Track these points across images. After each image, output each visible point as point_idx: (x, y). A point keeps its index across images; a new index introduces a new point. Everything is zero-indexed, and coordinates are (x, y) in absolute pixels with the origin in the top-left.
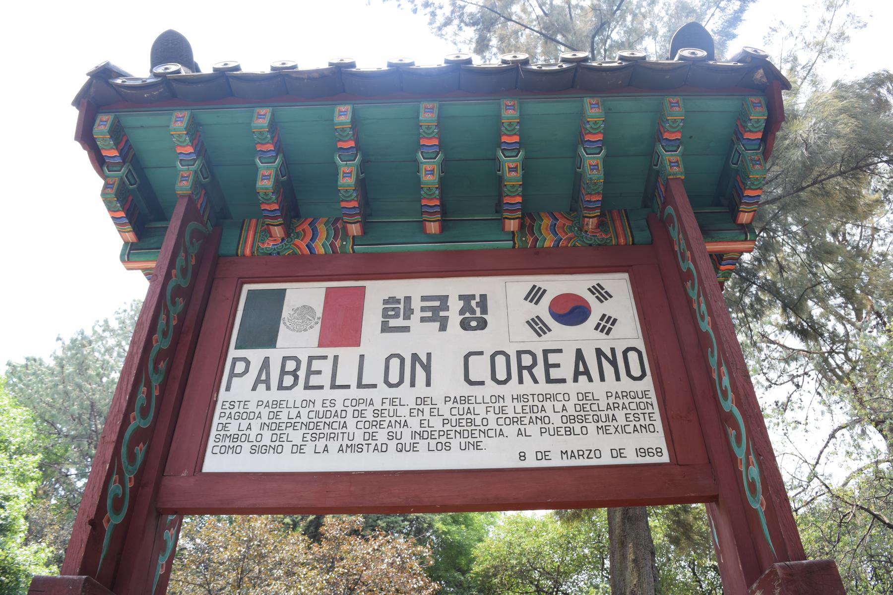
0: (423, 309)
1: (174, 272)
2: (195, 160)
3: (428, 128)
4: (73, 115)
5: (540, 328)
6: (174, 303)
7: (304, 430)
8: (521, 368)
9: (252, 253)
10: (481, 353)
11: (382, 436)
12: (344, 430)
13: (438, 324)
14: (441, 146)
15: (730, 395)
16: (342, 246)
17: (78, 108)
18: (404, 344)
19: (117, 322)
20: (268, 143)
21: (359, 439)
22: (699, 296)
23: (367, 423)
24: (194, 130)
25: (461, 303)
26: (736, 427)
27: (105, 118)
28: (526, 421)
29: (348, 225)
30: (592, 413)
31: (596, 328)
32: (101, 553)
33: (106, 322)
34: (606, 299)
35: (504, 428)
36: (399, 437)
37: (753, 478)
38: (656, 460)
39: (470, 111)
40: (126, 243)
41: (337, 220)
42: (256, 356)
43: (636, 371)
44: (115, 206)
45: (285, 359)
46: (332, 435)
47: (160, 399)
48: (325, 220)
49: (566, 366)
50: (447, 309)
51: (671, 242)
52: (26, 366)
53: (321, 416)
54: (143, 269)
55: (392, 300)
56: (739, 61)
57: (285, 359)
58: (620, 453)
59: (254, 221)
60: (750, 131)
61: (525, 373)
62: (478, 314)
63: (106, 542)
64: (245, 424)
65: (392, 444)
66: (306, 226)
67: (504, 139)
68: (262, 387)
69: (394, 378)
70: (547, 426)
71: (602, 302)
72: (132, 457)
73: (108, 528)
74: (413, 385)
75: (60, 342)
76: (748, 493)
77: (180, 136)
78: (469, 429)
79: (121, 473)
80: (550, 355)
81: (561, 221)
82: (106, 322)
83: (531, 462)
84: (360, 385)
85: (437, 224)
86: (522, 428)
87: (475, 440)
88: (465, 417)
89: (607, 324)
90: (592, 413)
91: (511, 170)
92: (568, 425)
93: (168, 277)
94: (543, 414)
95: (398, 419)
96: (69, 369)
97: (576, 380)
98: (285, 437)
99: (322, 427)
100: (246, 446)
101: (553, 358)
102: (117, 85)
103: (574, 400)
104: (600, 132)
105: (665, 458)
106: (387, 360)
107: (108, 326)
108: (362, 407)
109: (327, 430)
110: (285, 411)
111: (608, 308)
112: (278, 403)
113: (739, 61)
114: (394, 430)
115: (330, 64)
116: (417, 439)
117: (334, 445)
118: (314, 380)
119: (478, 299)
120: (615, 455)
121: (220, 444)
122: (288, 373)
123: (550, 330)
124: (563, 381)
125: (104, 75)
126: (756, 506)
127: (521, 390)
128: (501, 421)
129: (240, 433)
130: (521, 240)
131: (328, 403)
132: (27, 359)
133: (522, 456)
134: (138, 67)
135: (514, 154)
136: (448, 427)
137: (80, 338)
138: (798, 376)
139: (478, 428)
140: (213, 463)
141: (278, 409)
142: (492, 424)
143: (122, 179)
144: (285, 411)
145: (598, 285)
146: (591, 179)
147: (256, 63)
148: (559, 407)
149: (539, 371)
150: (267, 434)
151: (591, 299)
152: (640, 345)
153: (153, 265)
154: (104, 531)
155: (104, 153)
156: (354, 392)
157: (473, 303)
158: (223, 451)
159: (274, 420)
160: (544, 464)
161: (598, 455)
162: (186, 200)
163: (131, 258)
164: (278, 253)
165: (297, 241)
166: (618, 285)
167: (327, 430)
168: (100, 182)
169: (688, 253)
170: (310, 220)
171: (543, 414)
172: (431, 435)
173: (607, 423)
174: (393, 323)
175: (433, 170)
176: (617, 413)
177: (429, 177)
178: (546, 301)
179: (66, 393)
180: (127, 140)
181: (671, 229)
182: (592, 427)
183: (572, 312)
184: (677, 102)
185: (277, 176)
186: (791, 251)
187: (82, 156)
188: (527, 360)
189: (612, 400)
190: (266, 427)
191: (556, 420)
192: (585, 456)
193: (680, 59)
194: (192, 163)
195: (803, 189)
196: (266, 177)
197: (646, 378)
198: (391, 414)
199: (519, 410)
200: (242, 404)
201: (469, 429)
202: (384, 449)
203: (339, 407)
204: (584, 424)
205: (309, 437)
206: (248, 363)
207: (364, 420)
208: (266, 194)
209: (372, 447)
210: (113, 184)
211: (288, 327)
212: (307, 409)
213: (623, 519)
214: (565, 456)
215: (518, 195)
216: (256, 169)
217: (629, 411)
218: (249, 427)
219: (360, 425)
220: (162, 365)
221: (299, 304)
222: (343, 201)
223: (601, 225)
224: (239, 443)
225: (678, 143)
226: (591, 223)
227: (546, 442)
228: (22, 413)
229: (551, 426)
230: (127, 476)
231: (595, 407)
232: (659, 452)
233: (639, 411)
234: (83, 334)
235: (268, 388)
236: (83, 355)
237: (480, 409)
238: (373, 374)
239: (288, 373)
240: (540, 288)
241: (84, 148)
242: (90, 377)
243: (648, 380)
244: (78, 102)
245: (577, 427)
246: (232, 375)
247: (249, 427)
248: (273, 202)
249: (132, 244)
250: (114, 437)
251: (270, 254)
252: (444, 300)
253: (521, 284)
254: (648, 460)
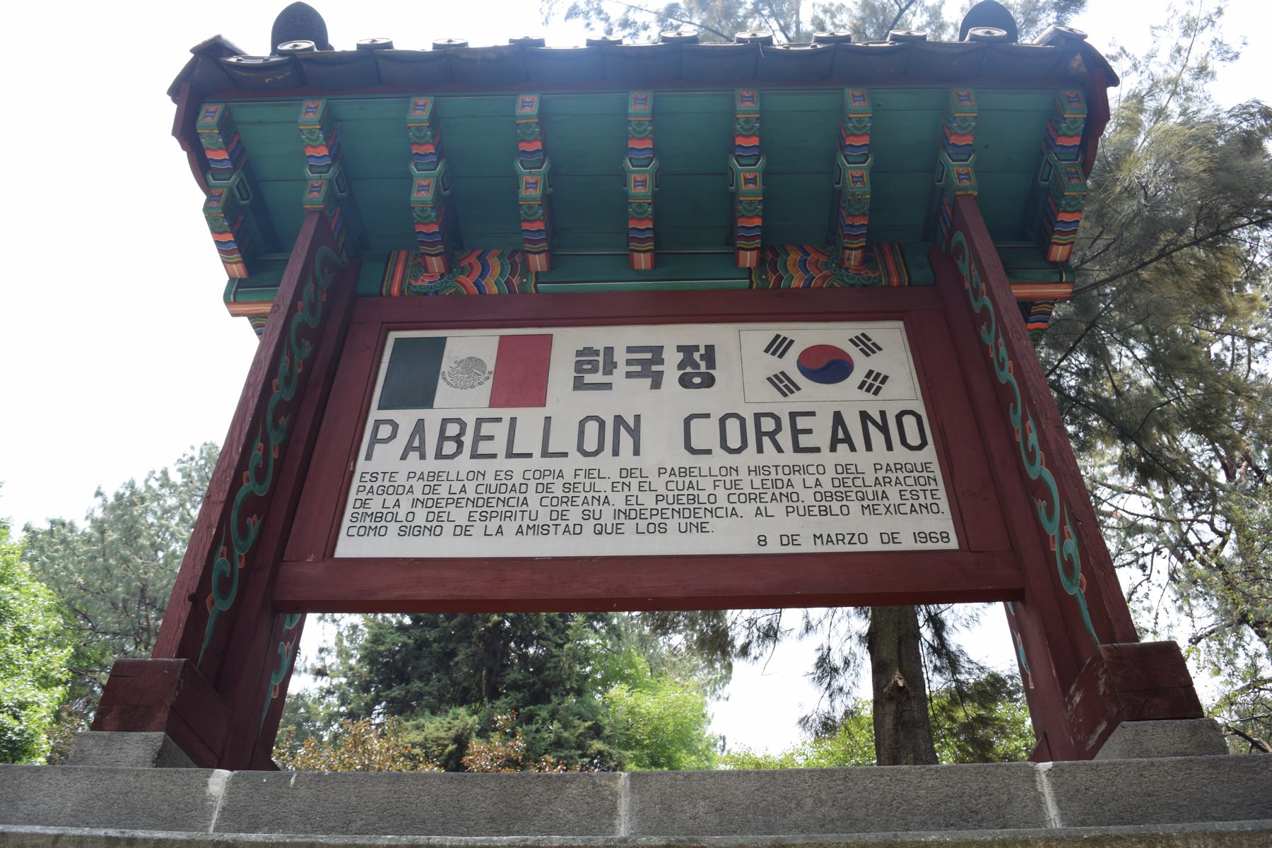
0: (629, 362)
1: (300, 304)
2: (329, 166)
3: (640, 124)
4: (170, 110)
5: (786, 386)
6: (299, 344)
7: (470, 507)
8: (760, 434)
9: (401, 292)
10: (707, 416)
11: (574, 515)
12: (525, 507)
13: (648, 381)
14: (655, 150)
15: (1039, 454)
16: (522, 285)
17: (175, 100)
18: (604, 405)
19: (180, 474)
20: (427, 143)
21: (544, 518)
22: (997, 338)
23: (555, 500)
24: (330, 124)
25: (681, 356)
26: (1047, 496)
27: (212, 108)
28: (767, 498)
29: (531, 256)
30: (855, 490)
31: (861, 387)
32: (202, 642)
33: (165, 473)
34: (874, 352)
35: (738, 506)
36: (597, 516)
37: (1070, 556)
38: (941, 546)
39: (696, 104)
40: (232, 279)
41: (515, 252)
42: (406, 418)
43: (914, 439)
44: (221, 226)
45: (445, 422)
46: (509, 514)
47: (279, 463)
48: (499, 252)
49: (821, 434)
50: (662, 362)
51: (960, 279)
52: (51, 533)
53: (493, 490)
54: (252, 317)
55: (589, 351)
56: (1049, 43)
57: (445, 422)
58: (893, 538)
59: (404, 253)
60: (1065, 135)
61: (766, 441)
62: (703, 369)
63: (209, 629)
64: (391, 501)
65: (589, 526)
66: (473, 259)
67: (740, 141)
68: (414, 456)
69: (590, 445)
70: (795, 505)
71: (868, 355)
72: (243, 531)
73: (212, 612)
74: (616, 453)
75: (100, 500)
76: (1063, 578)
77: (311, 132)
78: (691, 507)
79: (228, 543)
80: (799, 420)
81: (813, 256)
82: (165, 473)
83: (774, 547)
84: (545, 453)
85: (648, 255)
86: (762, 506)
87: (700, 521)
88: (685, 492)
89: (874, 383)
90: (855, 490)
91: (747, 181)
92: (823, 503)
93: (293, 309)
94: (790, 490)
95: (597, 495)
96: (112, 536)
97: (833, 449)
98: (445, 516)
99: (493, 505)
100: (393, 527)
101: (802, 423)
102: (231, 64)
103: (831, 472)
104: (865, 134)
105: (953, 544)
106: (582, 424)
107: (168, 480)
108: (549, 479)
109: (501, 508)
110: (446, 485)
111: (876, 363)
112: (435, 475)
113: (1049, 43)
114: (591, 508)
115: (511, 41)
116: (622, 519)
117: (510, 527)
118: (484, 448)
119: (702, 351)
120: (886, 540)
121: (358, 524)
122: (449, 438)
123: (798, 389)
124: (817, 450)
125: (213, 53)
126: (1073, 591)
127: (761, 460)
128: (733, 498)
129: (385, 511)
130: (760, 278)
131: (502, 475)
132: (53, 522)
133: (762, 540)
134: (255, 43)
135: (752, 162)
136: (663, 505)
137: (128, 493)
138: (1144, 555)
139: (703, 506)
140: (347, 547)
141: (435, 482)
142: (722, 501)
143: (231, 190)
144: (446, 485)
145: (863, 335)
146: (853, 194)
147: (414, 38)
148: (811, 481)
149: (785, 438)
150: (421, 513)
151: (854, 353)
152: (920, 408)
153: (267, 308)
154: (206, 615)
155: (210, 155)
156: (538, 462)
157: (696, 356)
158: (362, 532)
159: (431, 496)
160: (791, 549)
161: (863, 540)
162: (317, 217)
163: (239, 298)
164: (436, 292)
165: (463, 278)
166: (891, 338)
167: (501, 508)
168: (202, 197)
169: (983, 287)
170: (478, 252)
171: (790, 490)
172: (640, 515)
173: (875, 502)
174: (589, 378)
175: (645, 181)
176: (888, 489)
177: (640, 190)
178: (793, 354)
179: (108, 569)
180: (239, 141)
181: (960, 262)
182: (855, 506)
183: (827, 366)
184: (968, 95)
185: (437, 187)
186: (1129, 362)
187: (180, 158)
188: (768, 425)
189: (881, 474)
190: (419, 504)
191: (807, 497)
192: (846, 541)
193: (971, 39)
194: (325, 169)
195: (1143, 265)
196: (422, 188)
197: (926, 448)
198: (587, 488)
199: (757, 484)
200: (387, 476)
201: (691, 507)
202: (578, 531)
203: (517, 479)
204: (844, 502)
205: (477, 516)
206: (396, 427)
207: (551, 495)
208: (423, 210)
209: (561, 529)
210: (220, 196)
211: (449, 383)
212: (475, 483)
213: (895, 725)
214: (819, 541)
215: (757, 216)
216: (410, 177)
217: (904, 487)
218: (397, 504)
219: (546, 502)
220: (283, 421)
221: (464, 356)
222: (525, 221)
223: (866, 261)
224: (383, 523)
225: (970, 149)
226: (854, 257)
227: (793, 524)
228: (43, 593)
229: (799, 504)
230: (237, 552)
231: (859, 482)
232: (945, 537)
233: (918, 488)
234: (132, 487)
235: (423, 457)
236: (132, 515)
237: (706, 483)
238: (563, 439)
239: (449, 438)
240: (785, 339)
241: (184, 148)
242: (142, 547)
243: (930, 450)
244: (175, 91)
245: (835, 506)
246: (375, 440)
247: (397, 504)
248: (432, 222)
249: (241, 280)
250: (223, 496)
251: (425, 294)
252: (657, 351)
253: (761, 334)
254: (930, 546)
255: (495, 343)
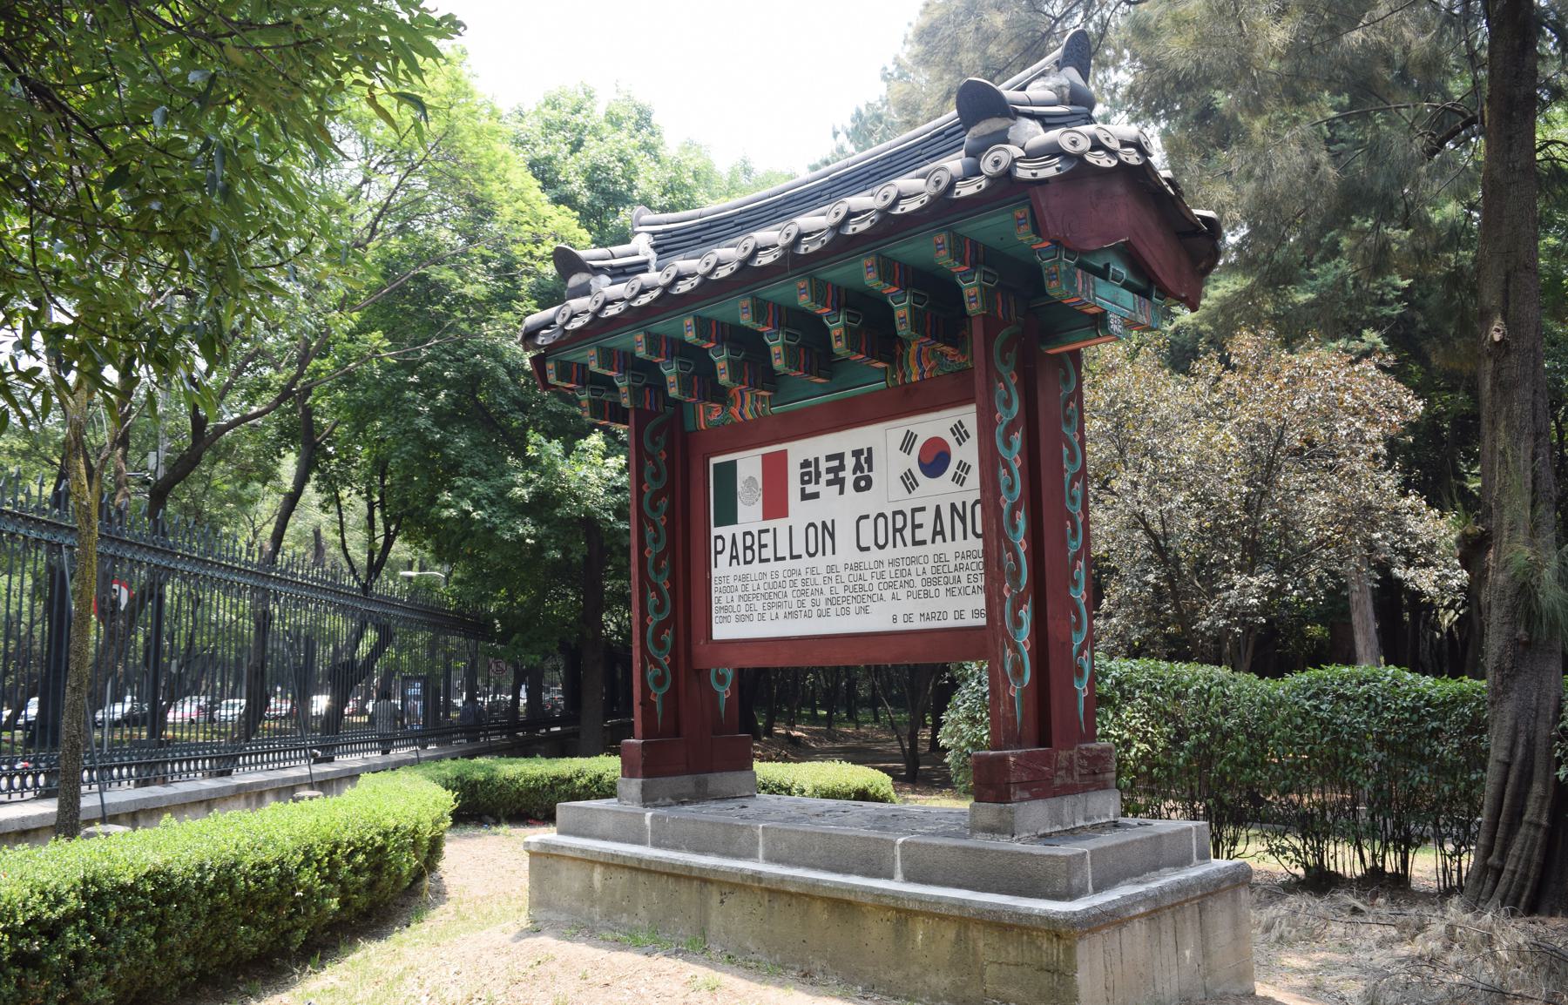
73: (657, 700)
142: (876, 590)
148: (920, 568)
246: (717, 553)
255: (759, 460)
